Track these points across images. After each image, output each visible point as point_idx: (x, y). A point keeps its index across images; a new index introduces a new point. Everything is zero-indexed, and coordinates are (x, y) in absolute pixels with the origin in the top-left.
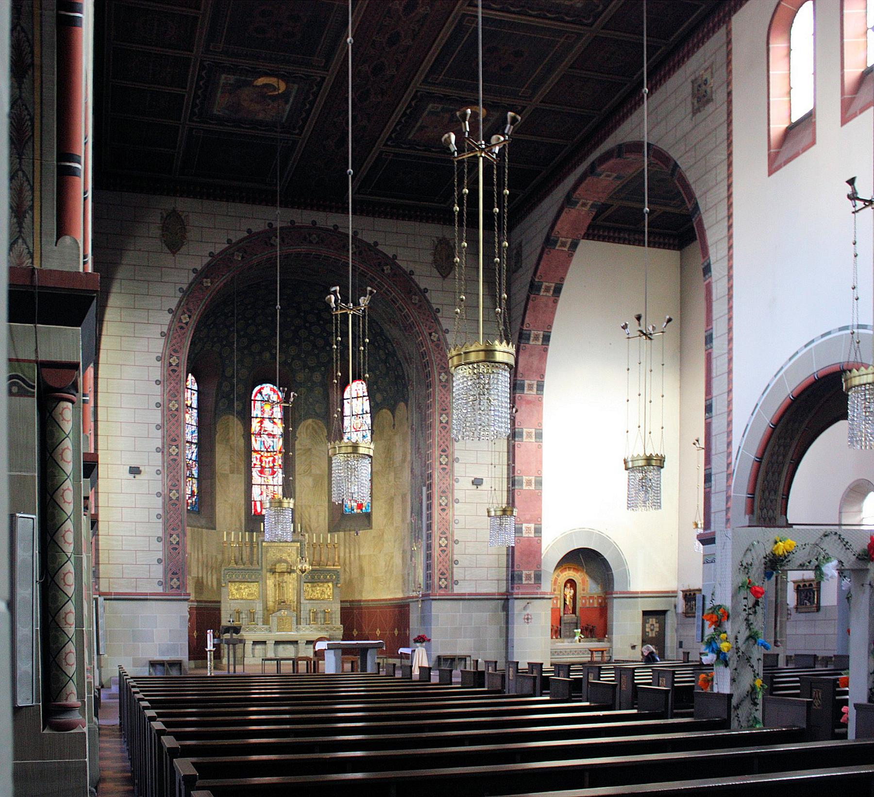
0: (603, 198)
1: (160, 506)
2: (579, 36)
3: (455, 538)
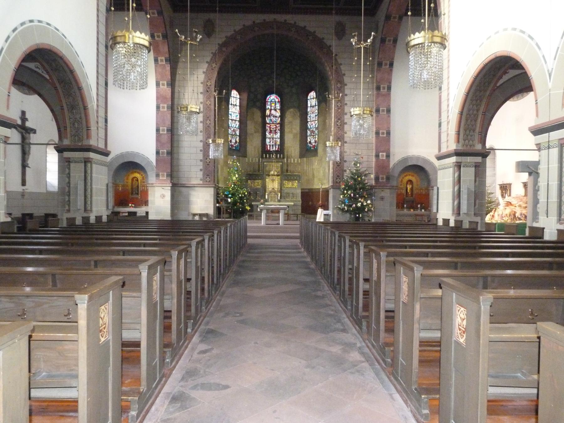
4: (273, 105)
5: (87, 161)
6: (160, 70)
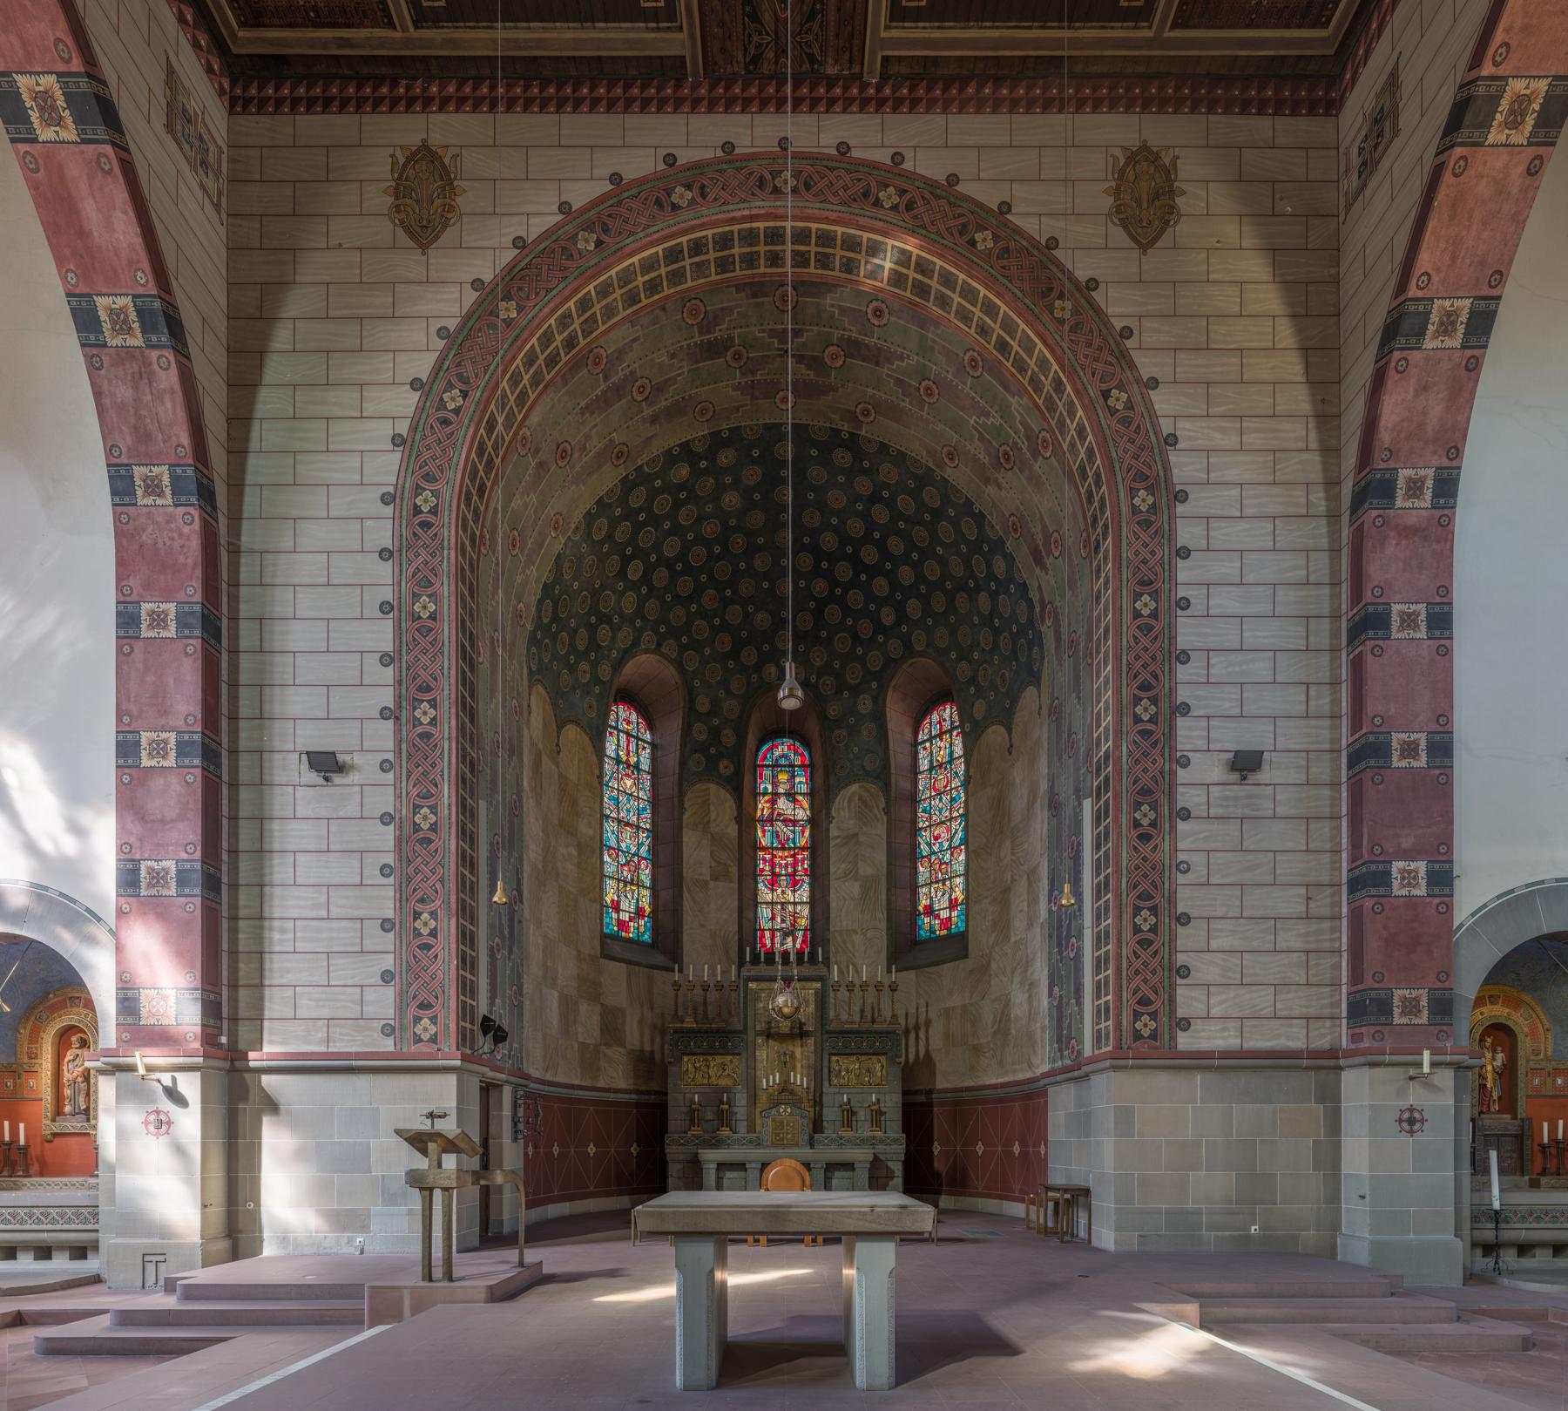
1: (390, 845)
3: (1180, 909)
4: (783, 777)
6: (124, 393)
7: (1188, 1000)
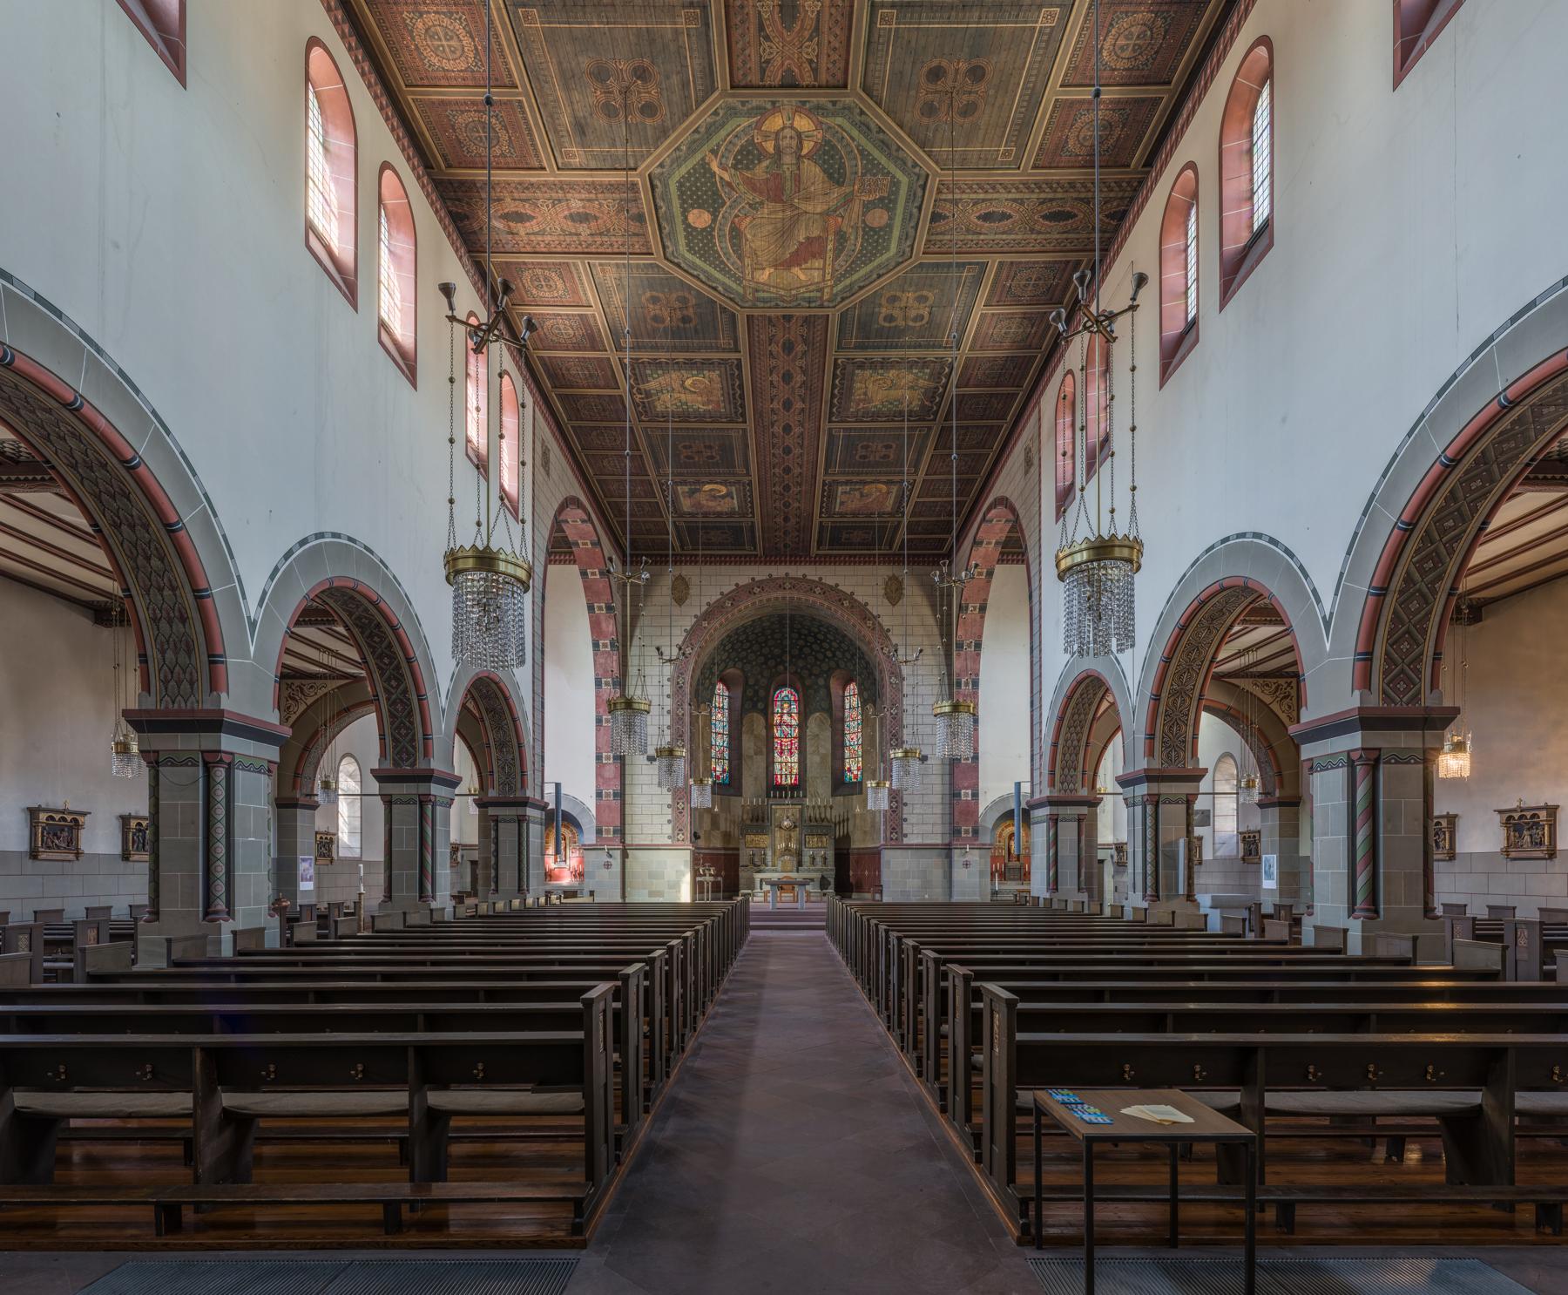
0: (1003, 537)
2: (930, 428)
5: (211, 760)
7: (906, 828)
